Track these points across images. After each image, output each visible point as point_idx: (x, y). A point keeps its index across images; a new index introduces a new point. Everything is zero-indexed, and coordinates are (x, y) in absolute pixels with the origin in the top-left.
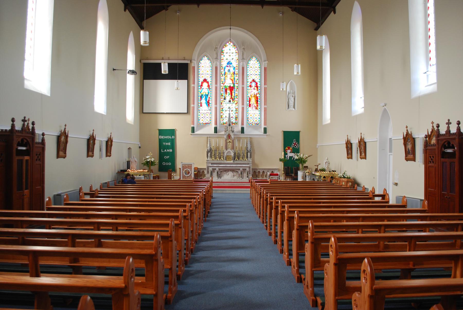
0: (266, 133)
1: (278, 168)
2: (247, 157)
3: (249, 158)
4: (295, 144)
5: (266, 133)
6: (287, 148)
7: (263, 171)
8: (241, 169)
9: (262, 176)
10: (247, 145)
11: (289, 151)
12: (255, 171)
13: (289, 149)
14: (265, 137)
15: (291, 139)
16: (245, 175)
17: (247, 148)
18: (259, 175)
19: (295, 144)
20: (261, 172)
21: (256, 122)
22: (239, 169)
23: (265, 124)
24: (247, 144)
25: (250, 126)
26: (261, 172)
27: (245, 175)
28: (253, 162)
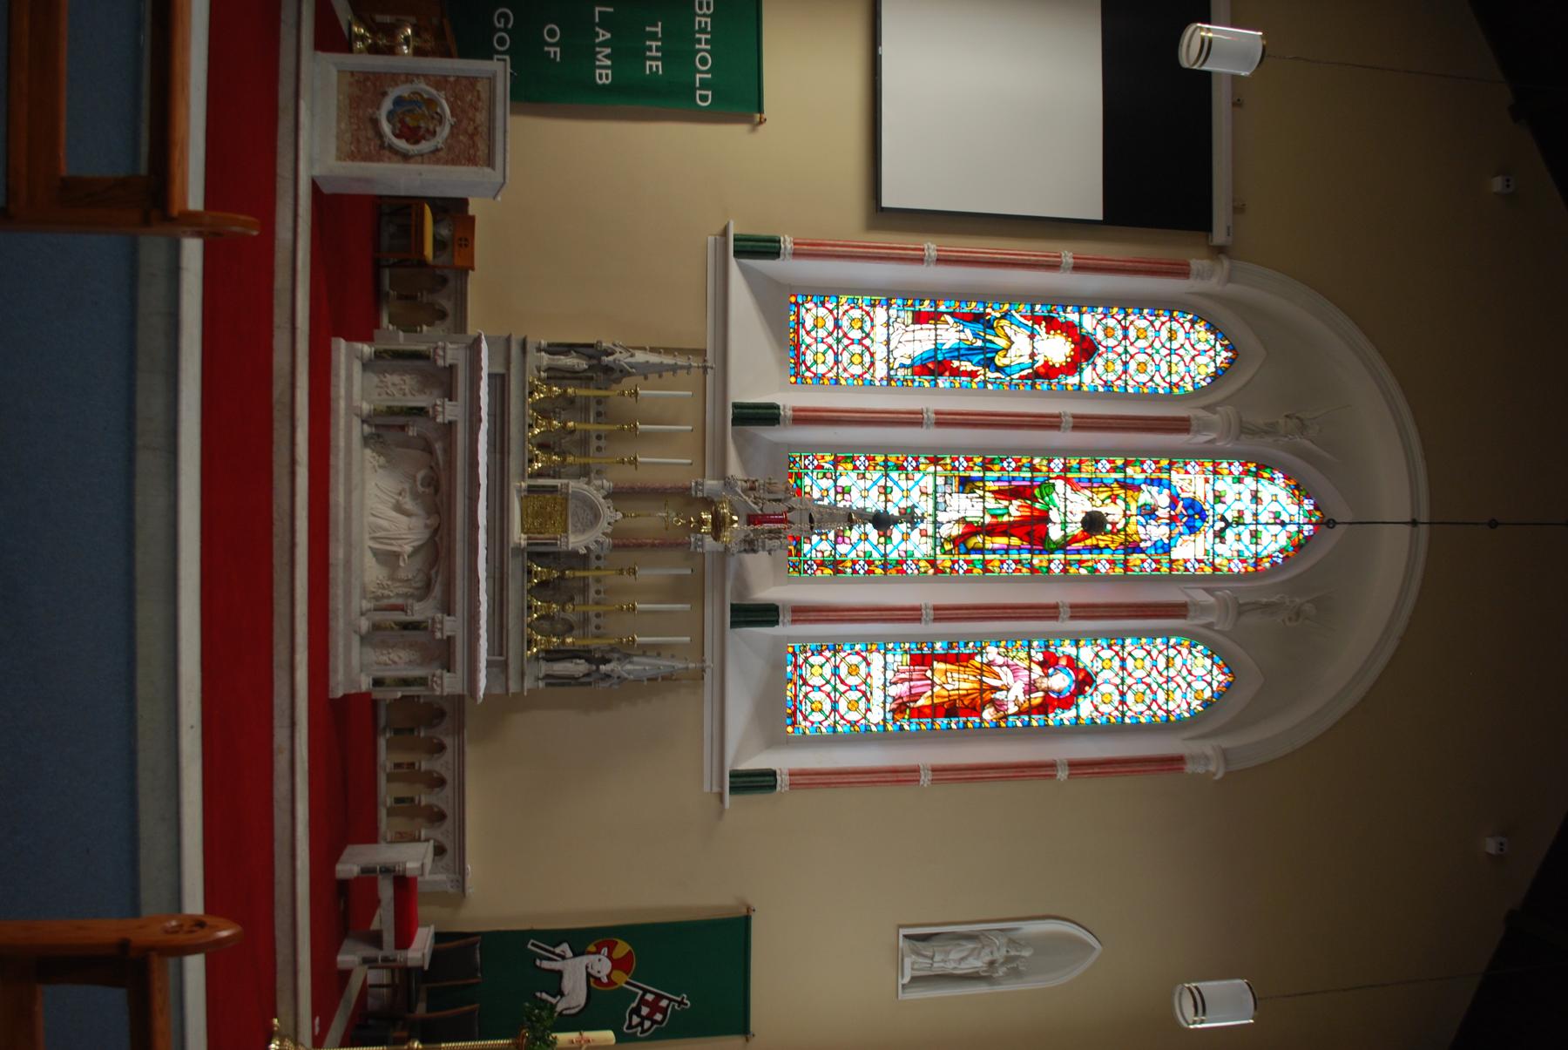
0: (734, 789)
2: (552, 655)
3: (545, 668)
5: (734, 789)
6: (622, 949)
7: (441, 782)
8: (452, 626)
9: (406, 773)
12: (441, 714)
13: (617, 964)
16: (400, 662)
17: (626, 651)
19: (654, 1007)
20: (440, 765)
22: (448, 609)
23: (806, 780)
24: (657, 650)
26: (440, 765)
27: (400, 662)
28: (503, 705)
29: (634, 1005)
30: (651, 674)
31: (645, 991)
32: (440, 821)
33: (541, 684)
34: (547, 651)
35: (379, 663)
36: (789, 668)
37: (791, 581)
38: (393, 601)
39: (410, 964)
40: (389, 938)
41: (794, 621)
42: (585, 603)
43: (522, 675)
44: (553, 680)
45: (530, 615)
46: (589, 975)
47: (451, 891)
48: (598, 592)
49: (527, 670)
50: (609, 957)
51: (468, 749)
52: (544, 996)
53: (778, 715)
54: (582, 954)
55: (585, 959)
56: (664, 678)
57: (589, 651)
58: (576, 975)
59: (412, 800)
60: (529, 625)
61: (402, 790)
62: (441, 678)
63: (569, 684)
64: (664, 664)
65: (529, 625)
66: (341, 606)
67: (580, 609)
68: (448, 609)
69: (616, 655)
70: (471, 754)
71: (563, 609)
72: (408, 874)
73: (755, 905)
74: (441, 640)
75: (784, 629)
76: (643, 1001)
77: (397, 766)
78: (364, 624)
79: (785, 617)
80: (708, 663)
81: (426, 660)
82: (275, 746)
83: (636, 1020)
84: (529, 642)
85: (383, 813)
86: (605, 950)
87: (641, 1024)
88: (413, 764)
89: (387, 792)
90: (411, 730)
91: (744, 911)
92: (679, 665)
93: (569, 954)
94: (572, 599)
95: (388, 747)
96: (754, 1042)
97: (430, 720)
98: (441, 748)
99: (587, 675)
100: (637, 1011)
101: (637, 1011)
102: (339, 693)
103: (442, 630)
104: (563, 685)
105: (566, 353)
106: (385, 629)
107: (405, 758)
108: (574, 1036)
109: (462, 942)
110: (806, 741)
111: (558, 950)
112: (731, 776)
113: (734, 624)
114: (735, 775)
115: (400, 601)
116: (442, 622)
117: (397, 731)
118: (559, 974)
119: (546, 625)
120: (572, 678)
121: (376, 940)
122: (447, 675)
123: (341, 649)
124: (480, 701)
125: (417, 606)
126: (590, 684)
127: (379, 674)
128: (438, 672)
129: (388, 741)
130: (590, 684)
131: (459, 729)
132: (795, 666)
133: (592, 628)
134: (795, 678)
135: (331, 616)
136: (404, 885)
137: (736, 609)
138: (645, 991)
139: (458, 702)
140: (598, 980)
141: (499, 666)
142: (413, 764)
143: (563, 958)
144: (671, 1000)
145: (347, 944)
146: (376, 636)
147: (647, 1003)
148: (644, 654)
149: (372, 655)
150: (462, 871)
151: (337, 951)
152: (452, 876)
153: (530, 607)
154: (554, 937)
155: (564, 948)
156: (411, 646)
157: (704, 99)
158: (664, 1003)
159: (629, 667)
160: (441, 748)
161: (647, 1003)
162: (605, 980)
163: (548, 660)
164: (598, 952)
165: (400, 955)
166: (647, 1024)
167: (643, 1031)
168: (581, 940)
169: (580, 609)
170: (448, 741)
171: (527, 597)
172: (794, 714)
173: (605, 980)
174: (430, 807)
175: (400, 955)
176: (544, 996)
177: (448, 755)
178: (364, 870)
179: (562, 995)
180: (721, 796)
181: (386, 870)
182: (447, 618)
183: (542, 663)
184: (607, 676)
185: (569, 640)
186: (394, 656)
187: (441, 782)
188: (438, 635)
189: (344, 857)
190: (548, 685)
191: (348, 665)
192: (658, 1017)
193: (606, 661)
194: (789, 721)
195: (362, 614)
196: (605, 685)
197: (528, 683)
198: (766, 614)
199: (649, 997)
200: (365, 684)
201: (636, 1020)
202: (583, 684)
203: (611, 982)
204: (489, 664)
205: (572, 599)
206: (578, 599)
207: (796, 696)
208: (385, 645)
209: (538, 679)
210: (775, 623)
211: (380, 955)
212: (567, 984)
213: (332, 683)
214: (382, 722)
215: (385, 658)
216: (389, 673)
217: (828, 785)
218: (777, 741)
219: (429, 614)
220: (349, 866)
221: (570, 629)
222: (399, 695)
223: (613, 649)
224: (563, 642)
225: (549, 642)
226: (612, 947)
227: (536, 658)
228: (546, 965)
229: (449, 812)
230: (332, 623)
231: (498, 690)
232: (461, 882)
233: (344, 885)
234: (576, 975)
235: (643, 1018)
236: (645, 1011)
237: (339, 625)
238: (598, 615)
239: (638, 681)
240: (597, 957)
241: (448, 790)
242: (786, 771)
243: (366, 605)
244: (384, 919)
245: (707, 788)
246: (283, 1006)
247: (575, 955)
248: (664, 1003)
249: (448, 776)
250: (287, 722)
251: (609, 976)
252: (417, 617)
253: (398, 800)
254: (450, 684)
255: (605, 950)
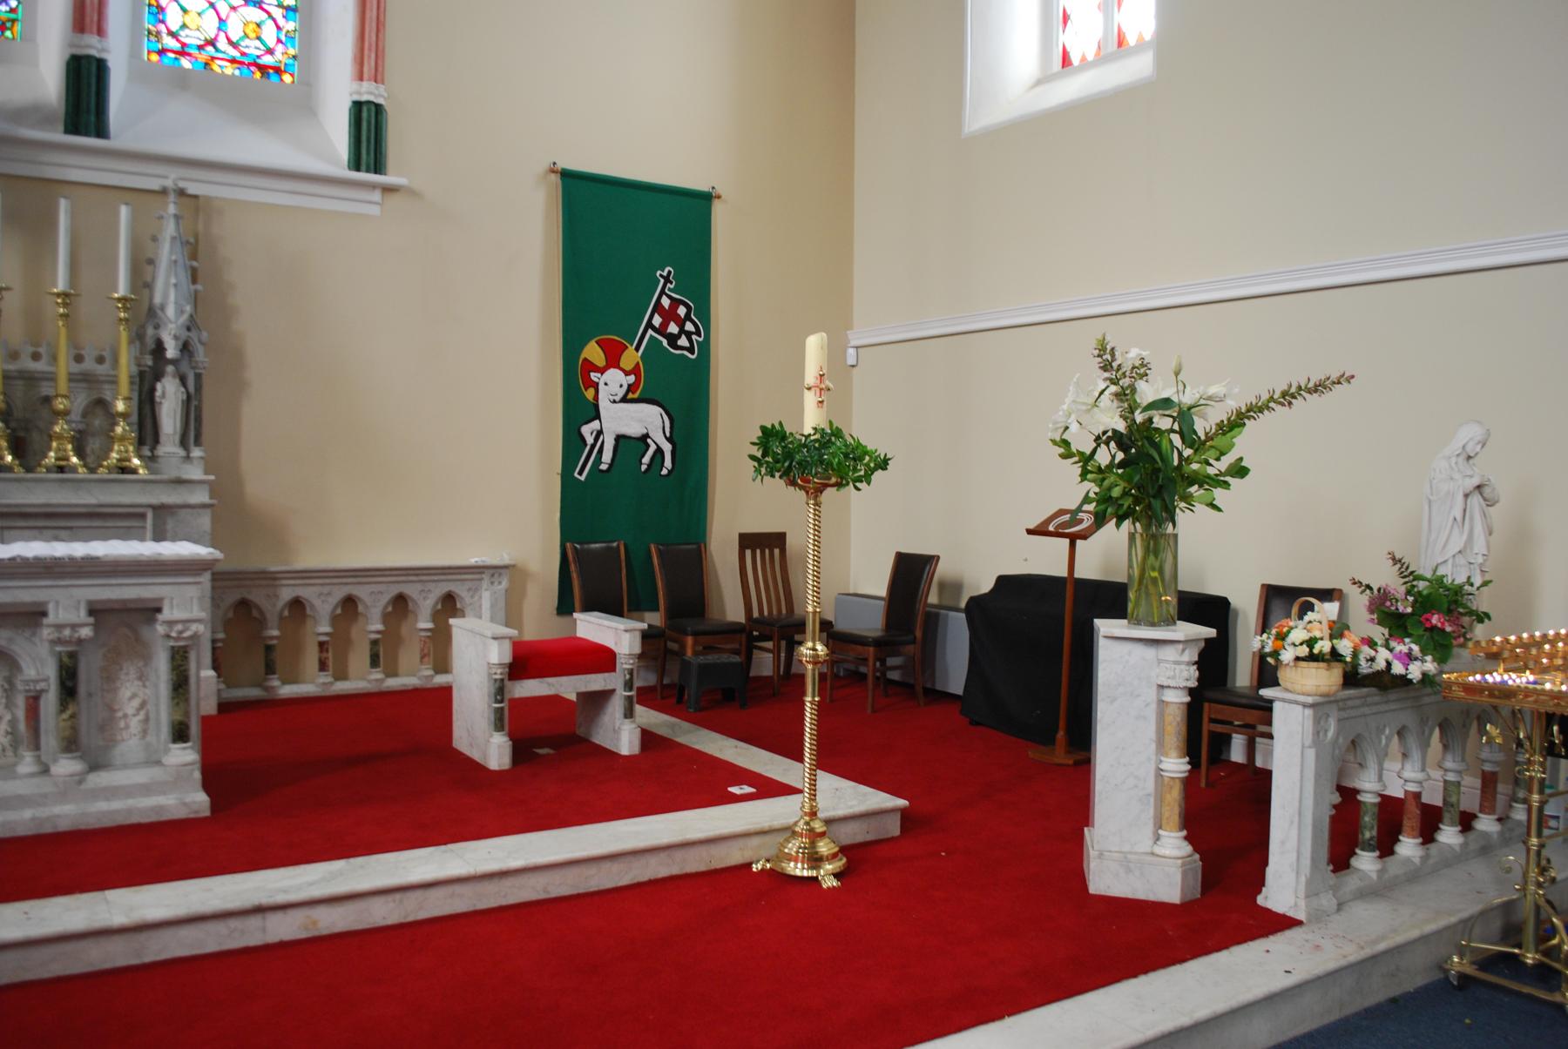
0: (378, 167)
1: (505, 559)
2: (147, 432)
3: (169, 446)
4: (669, 315)
5: (378, 167)
6: (593, 353)
7: (350, 603)
8: (67, 608)
9: (332, 655)
10: (142, 267)
11: (613, 382)
12: (244, 605)
13: (613, 361)
14: (369, 206)
15: (630, 259)
16: (139, 697)
17: (141, 313)
18: (297, 649)
19: (669, 315)
20: (323, 604)
21: (253, 49)
22: (33, 616)
23: (370, 54)
24: (142, 267)
25: (182, 80)
26: (323, 604)
27: (139, 697)
28: (230, 512)
29: (665, 342)
30: (184, 277)
31: (650, 325)
32: (424, 603)
33: (196, 453)
34: (141, 442)
35: (145, 732)
36: (185, 63)
37: (29, 37)
38: (21, 713)
39: (637, 650)
40: (596, 682)
41: (101, 32)
42: (52, 378)
43: (180, 482)
44: (192, 432)
45: (74, 469)
46: (624, 400)
47: (505, 584)
48: (36, 357)
49: (173, 474)
50: (602, 371)
51: (301, 564)
52: (646, 460)
53: (262, 85)
54: (596, 407)
55: (604, 404)
56: (194, 256)
57: (141, 374)
58: (625, 417)
59: (375, 643)
60: (92, 470)
61: (359, 658)
62: (171, 623)
63: (199, 409)
64: (166, 252)
65: (92, 470)
66: (28, 814)
67: (63, 385)
68: (33, 616)
69: (150, 331)
70: (310, 558)
71: (65, 413)
72: (508, 659)
73: (546, 164)
74: (97, 627)
75: (115, 49)
76: (661, 331)
77: (323, 666)
78: (66, 766)
79: (91, 45)
80: (169, 183)
81: (142, 652)
82: (303, 935)
83: (683, 341)
84: (123, 470)
85: (393, 683)
86: (594, 376)
87: (689, 335)
88: (321, 645)
89: (361, 679)
90: (269, 649)
91: (555, 178)
92: (170, 229)
93: (595, 425)
94: (47, 400)
95: (295, 681)
96: (719, 190)
97: (251, 617)
98: (297, 605)
99: (183, 380)
100: (672, 339)
101: (672, 339)
102: (197, 801)
103: (74, 627)
104: (199, 420)
105: (1255, 787)
106: (75, 729)
107: (311, 657)
108: (810, 399)
109: (573, 567)
110: (308, 53)
111: (590, 440)
112: (358, 169)
113: (101, 131)
114: (356, 164)
115: (20, 701)
116: (59, 627)
117: (270, 669)
118: (620, 438)
119: (93, 445)
120: (187, 402)
121: (597, 700)
122: (166, 614)
123: (116, 805)
124: (217, 554)
125: (30, 672)
126: (198, 377)
127: (165, 731)
128: (161, 629)
129: (285, 682)
130: (198, 377)
131: (269, 579)
132: (182, 53)
133: (102, 370)
134: (203, 56)
135: (47, 829)
136: (525, 661)
137: (75, 124)
138: (650, 325)
139: (221, 578)
140: (631, 388)
141: (162, 520)
142: (321, 645)
143: (600, 433)
144: (662, 292)
145: (601, 738)
146: (88, 746)
147: (665, 325)
148: (149, 286)
149: (130, 744)
150: (479, 570)
151: (614, 756)
152: (485, 584)
153: (61, 469)
154: (573, 443)
155: (588, 431)
156: (110, 678)
157: (149, 534)
158: (666, 302)
159: (171, 311)
160: (297, 605)
161: (665, 325)
162: (632, 379)
163: (156, 440)
164: (596, 386)
165: (624, 663)
166: (689, 327)
167: (698, 333)
168: (579, 408)
169: (63, 385)
170: (286, 594)
171: (41, 473)
172: (263, 69)
173: (632, 379)
174: (386, 618)
175: (624, 663)
176: (646, 460)
177: (306, 593)
178: (499, 726)
179: (647, 436)
180: (388, 190)
181: (500, 692)
182: (51, 618)
183: (162, 450)
184: (185, 348)
185: (120, 406)
186: (130, 708)
187: (350, 603)
188: (86, 632)
189: (476, 755)
190: (198, 443)
191: (146, 789)
192: (682, 311)
193: (159, 348)
194: (274, 78)
195: (45, 771)
196: (201, 355)
197: (195, 472)
198: (86, 86)
199: (657, 321)
200: (185, 756)
201: (683, 341)
202: (199, 388)
203: (635, 371)
204: (159, 537)
205: (47, 400)
206: (46, 390)
207: (233, 61)
208: (108, 725)
209: (188, 458)
210: (101, 67)
211: (621, 693)
212: (635, 430)
213: (181, 814)
214: (253, 693)
215: (135, 724)
216: (164, 715)
217: (380, 25)
218: (305, 102)
219: (44, 650)
220: (495, 752)
221: (102, 405)
222: (209, 673)
223: (138, 337)
224: (124, 416)
225: (122, 439)
226: (589, 366)
227: (151, 460)
228: (607, 456)
229: (395, 590)
230: (64, 826)
231: (205, 521)
232: (495, 570)
233: (521, 750)
234: (625, 417)
235: (682, 331)
236: (673, 328)
237: (67, 814)
238: (79, 359)
239: (196, 299)
240: (601, 386)
241: (361, 592)
242: (355, 86)
243: (27, 765)
244: (568, 687)
245: (375, 210)
246: (732, 856)
247: (598, 416)
248: (666, 302)
249: (340, 593)
250: (254, 922)
251: (627, 373)
252: (51, 671)
253: (375, 661)
254: (187, 610)
255: (594, 376)
